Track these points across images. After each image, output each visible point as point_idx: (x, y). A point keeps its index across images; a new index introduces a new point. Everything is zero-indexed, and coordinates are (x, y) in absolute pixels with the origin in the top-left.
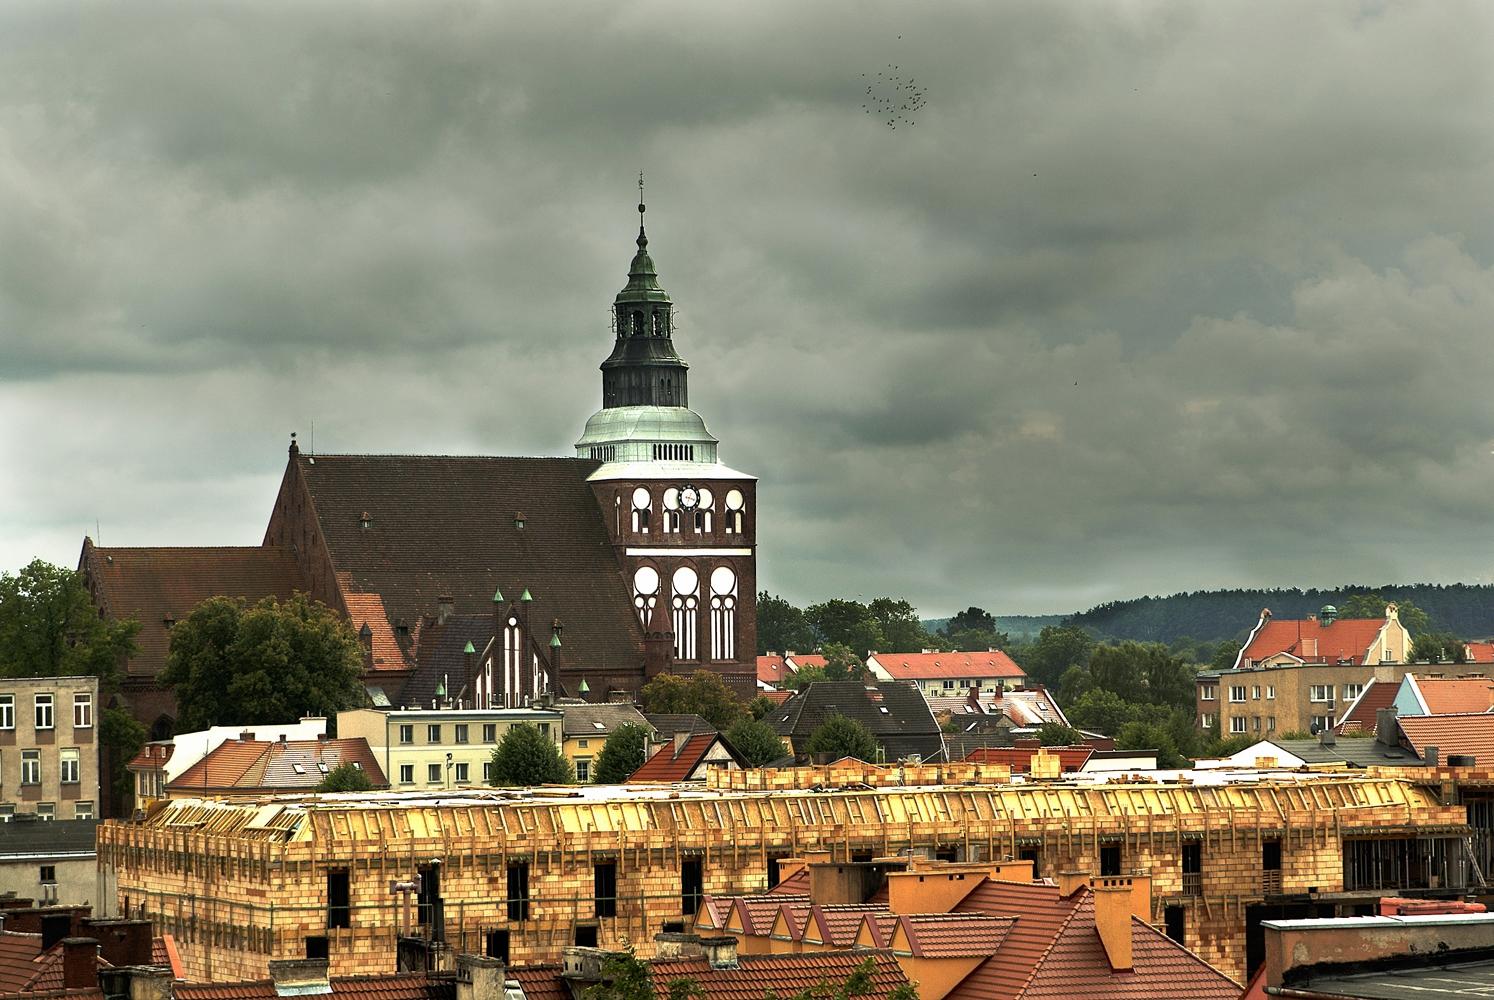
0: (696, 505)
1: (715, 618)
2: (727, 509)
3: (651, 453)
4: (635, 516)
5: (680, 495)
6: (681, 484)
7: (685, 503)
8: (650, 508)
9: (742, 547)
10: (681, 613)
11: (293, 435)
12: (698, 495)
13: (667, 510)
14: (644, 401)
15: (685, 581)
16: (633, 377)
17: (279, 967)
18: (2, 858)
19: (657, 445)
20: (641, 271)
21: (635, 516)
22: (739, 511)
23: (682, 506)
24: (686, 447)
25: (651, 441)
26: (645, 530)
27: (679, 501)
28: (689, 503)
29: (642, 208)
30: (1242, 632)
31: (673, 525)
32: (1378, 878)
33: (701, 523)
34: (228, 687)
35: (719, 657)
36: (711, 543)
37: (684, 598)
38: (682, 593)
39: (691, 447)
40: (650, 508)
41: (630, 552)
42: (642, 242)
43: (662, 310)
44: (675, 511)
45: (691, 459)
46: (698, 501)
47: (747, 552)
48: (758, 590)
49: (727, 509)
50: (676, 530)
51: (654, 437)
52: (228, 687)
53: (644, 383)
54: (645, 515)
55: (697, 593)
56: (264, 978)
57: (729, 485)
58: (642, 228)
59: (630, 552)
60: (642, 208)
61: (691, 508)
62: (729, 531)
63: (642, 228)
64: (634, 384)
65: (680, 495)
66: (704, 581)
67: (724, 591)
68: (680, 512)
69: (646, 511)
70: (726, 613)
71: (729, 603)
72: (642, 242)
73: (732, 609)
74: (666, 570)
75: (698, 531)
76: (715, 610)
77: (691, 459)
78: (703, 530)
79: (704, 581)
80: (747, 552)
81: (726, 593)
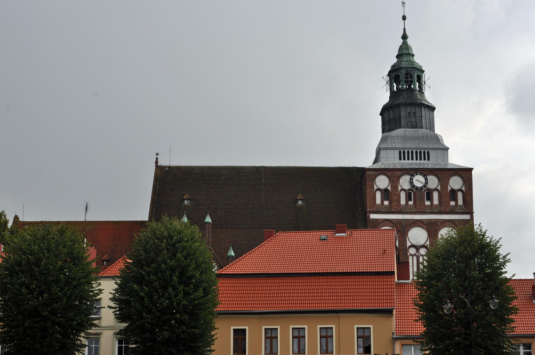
0: (424, 186)
2: (449, 188)
3: (397, 155)
6: (412, 172)
8: (389, 188)
10: (415, 258)
11: (157, 154)
12: (426, 179)
13: (403, 190)
14: (397, 126)
16: (391, 113)
18: (313, 350)
19: (402, 151)
20: (404, 52)
21: (378, 195)
22: (460, 190)
23: (413, 186)
24: (424, 152)
26: (386, 203)
27: (411, 183)
28: (418, 185)
29: (404, 18)
31: (409, 198)
33: (430, 197)
36: (437, 211)
37: (417, 248)
39: (428, 153)
40: (389, 188)
41: (373, 216)
42: (405, 37)
44: (409, 190)
45: (429, 159)
46: (427, 183)
47: (467, 217)
49: (449, 188)
50: (411, 203)
51: (400, 146)
53: (397, 115)
54: (385, 193)
56: (83, 334)
57: (451, 172)
58: (404, 29)
59: (373, 216)
60: (404, 18)
61: (421, 187)
62: (453, 203)
63: (404, 29)
64: (391, 117)
65: (412, 179)
68: (413, 190)
69: (386, 190)
71: (423, 251)
72: (405, 37)
75: (428, 203)
77: (429, 159)
78: (457, 203)
80: (467, 217)
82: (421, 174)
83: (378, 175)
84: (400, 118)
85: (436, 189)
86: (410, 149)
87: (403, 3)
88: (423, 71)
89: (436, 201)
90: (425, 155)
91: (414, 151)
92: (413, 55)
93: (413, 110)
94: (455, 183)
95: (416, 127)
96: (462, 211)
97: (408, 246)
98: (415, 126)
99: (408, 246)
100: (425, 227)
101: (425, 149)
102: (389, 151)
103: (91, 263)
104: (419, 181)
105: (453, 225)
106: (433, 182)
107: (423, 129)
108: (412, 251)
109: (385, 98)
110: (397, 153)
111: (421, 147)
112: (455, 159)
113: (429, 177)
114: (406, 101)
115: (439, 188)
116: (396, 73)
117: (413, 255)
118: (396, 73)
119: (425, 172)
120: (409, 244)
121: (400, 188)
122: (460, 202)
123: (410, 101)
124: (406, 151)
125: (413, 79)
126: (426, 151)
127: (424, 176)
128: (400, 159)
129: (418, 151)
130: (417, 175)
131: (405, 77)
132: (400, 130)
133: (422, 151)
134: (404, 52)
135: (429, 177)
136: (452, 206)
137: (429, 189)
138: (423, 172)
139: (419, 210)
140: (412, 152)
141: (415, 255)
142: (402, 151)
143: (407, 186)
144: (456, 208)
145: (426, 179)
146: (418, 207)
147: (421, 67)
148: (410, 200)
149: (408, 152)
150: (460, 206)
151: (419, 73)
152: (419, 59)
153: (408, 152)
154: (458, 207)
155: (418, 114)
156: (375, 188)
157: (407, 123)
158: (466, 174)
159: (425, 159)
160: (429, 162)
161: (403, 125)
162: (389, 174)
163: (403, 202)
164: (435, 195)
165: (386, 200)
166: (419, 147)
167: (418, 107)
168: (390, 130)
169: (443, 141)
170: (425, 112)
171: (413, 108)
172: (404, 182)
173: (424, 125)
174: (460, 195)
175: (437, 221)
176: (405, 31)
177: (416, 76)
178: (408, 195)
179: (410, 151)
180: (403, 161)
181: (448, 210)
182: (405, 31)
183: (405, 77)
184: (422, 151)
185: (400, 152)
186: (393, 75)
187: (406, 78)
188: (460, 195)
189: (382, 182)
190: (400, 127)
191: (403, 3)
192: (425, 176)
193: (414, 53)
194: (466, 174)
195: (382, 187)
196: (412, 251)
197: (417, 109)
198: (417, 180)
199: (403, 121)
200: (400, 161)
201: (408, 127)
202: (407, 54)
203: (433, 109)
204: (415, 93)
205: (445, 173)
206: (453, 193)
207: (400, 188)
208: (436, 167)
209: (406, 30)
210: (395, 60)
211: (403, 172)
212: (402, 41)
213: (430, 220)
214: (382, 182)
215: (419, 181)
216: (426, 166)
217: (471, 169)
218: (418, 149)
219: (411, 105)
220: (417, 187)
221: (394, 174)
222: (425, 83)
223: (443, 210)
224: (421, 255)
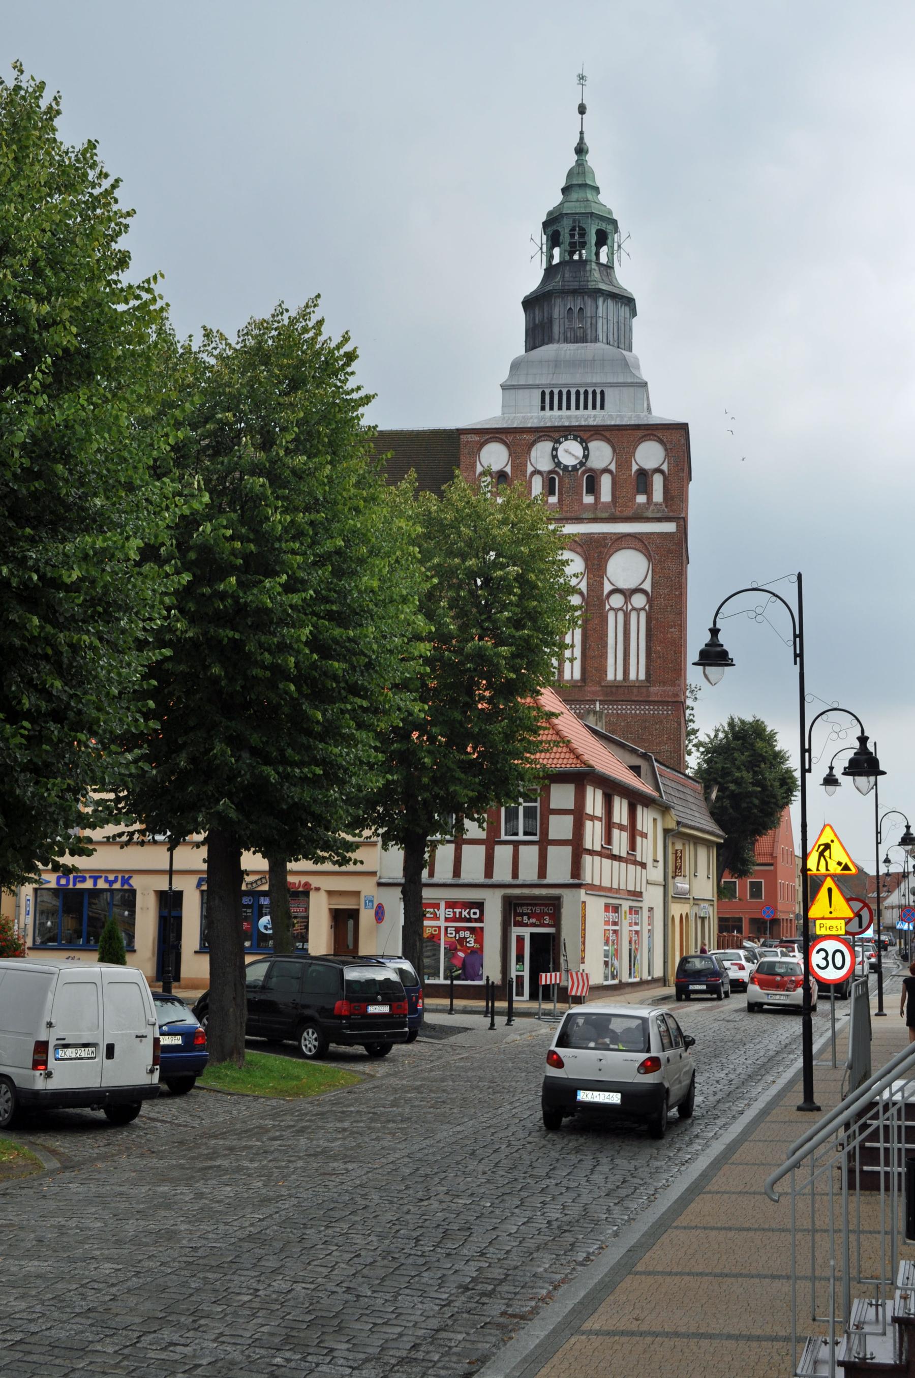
0: (582, 464)
2: (635, 468)
5: (555, 449)
7: (561, 460)
8: (508, 469)
9: (659, 520)
10: (621, 615)
12: (586, 449)
13: (536, 472)
16: (537, 312)
17: (167, 989)
19: (547, 391)
20: (578, 182)
22: (658, 470)
23: (558, 464)
24: (594, 393)
25: (537, 386)
27: (555, 457)
28: (568, 460)
29: (582, 110)
32: (520, 959)
33: (593, 487)
35: (620, 677)
36: (605, 515)
37: (628, 594)
38: (622, 585)
39: (602, 393)
42: (581, 150)
44: (550, 472)
45: (602, 407)
46: (586, 457)
47: (670, 527)
50: (553, 500)
51: (544, 381)
57: (640, 433)
58: (582, 133)
60: (582, 110)
61: (574, 467)
62: (641, 499)
63: (582, 133)
65: (555, 449)
70: (634, 616)
71: (639, 601)
72: (581, 150)
74: (597, 553)
75: (588, 499)
78: (649, 499)
80: (670, 527)
81: (632, 585)
82: (575, 439)
83: (487, 442)
84: (551, 321)
85: (606, 470)
86: (565, 385)
87: (582, 78)
88: (614, 222)
89: (606, 496)
90: (597, 399)
91: (573, 391)
92: (597, 190)
93: (579, 303)
94: (649, 455)
95: (584, 340)
96: (659, 515)
97: (606, 592)
98: (581, 339)
99: (606, 592)
100: (579, 550)
101: (595, 385)
102: (521, 391)
104: (570, 452)
105: (639, 545)
106: (601, 454)
107: (598, 345)
108: (617, 601)
110: (537, 394)
111: (589, 381)
112: (663, 410)
113: (592, 445)
114: (575, 287)
115: (613, 467)
116: (555, 227)
117: (616, 610)
118: (555, 227)
119: (584, 434)
120: (607, 587)
121: (530, 469)
122: (658, 496)
123: (575, 285)
124: (556, 391)
125: (586, 239)
126: (598, 391)
127: (581, 443)
128: (543, 408)
129: (582, 391)
130: (566, 439)
132: (550, 346)
133: (590, 391)
134: (578, 182)
135: (592, 445)
136: (639, 504)
137: (591, 470)
138: (581, 434)
139: (568, 515)
140: (569, 393)
141: (621, 609)
142: (547, 391)
143: (545, 465)
144: (647, 509)
145: (586, 449)
146: (565, 509)
147: (610, 212)
148: (552, 492)
149: (560, 393)
150: (656, 504)
151: (603, 226)
153: (560, 393)
154: (652, 507)
155: (588, 312)
156: (479, 469)
157: (565, 333)
158: (675, 437)
159: (594, 407)
160: (603, 413)
161: (556, 337)
162: (509, 439)
164: (606, 483)
166: (584, 381)
167: (590, 296)
168: (534, 348)
169: (638, 367)
170: (604, 308)
171: (579, 301)
172: (540, 457)
173: (601, 335)
174: (658, 482)
175: (604, 536)
176: (582, 139)
177: (593, 231)
178: (547, 483)
179: (565, 391)
180: (548, 413)
181: (629, 513)
182: (582, 139)
184: (590, 391)
185: (543, 393)
186: (550, 230)
187: (572, 236)
188: (658, 482)
189: (495, 457)
190: (550, 341)
191: (582, 78)
192: (584, 443)
193: (598, 183)
194: (675, 437)
195: (495, 468)
197: (589, 301)
198: (566, 451)
199: (556, 329)
200: (543, 413)
201: (566, 341)
202: (580, 186)
203: (628, 302)
204: (588, 268)
206: (643, 478)
207: (530, 469)
208: (609, 423)
209: (585, 136)
210: (559, 198)
211: (538, 435)
212: (575, 157)
213: (589, 535)
214: (495, 457)
215: (570, 452)
216: (591, 422)
217: (683, 428)
218: (581, 385)
219: (575, 292)
220: (566, 467)
221: (517, 439)
222: (619, 246)
223: (618, 513)
224: (634, 609)
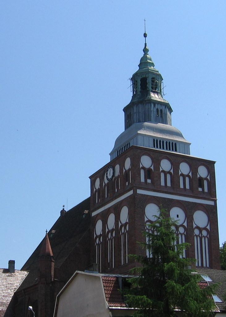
1: (196, 241)
4: (142, 172)
8: (152, 168)
15: (177, 215)
20: (144, 62)
21: (142, 172)
26: (149, 181)
29: (145, 35)
30: (47, 241)
34: (148, 257)
37: (200, 230)
38: (204, 235)
40: (152, 168)
42: (146, 51)
43: (148, 50)
47: (212, 203)
48: (220, 247)
49: (198, 176)
52: (148, 257)
54: (149, 173)
55: (185, 224)
58: (146, 44)
60: (145, 35)
63: (146, 44)
66: (189, 218)
67: (202, 225)
70: (180, 236)
72: (146, 51)
73: (207, 237)
76: (197, 236)
79: (189, 218)
80: (212, 203)
94: (202, 172)
97: (194, 227)
103: (150, 302)
109: (132, 96)
122: (206, 190)
131: (145, 82)
152: (159, 66)
163: (143, 180)
165: (150, 178)
174: (205, 183)
183: (145, 82)
196: (197, 232)
205: (195, 163)
206: (201, 180)
217: (214, 162)
